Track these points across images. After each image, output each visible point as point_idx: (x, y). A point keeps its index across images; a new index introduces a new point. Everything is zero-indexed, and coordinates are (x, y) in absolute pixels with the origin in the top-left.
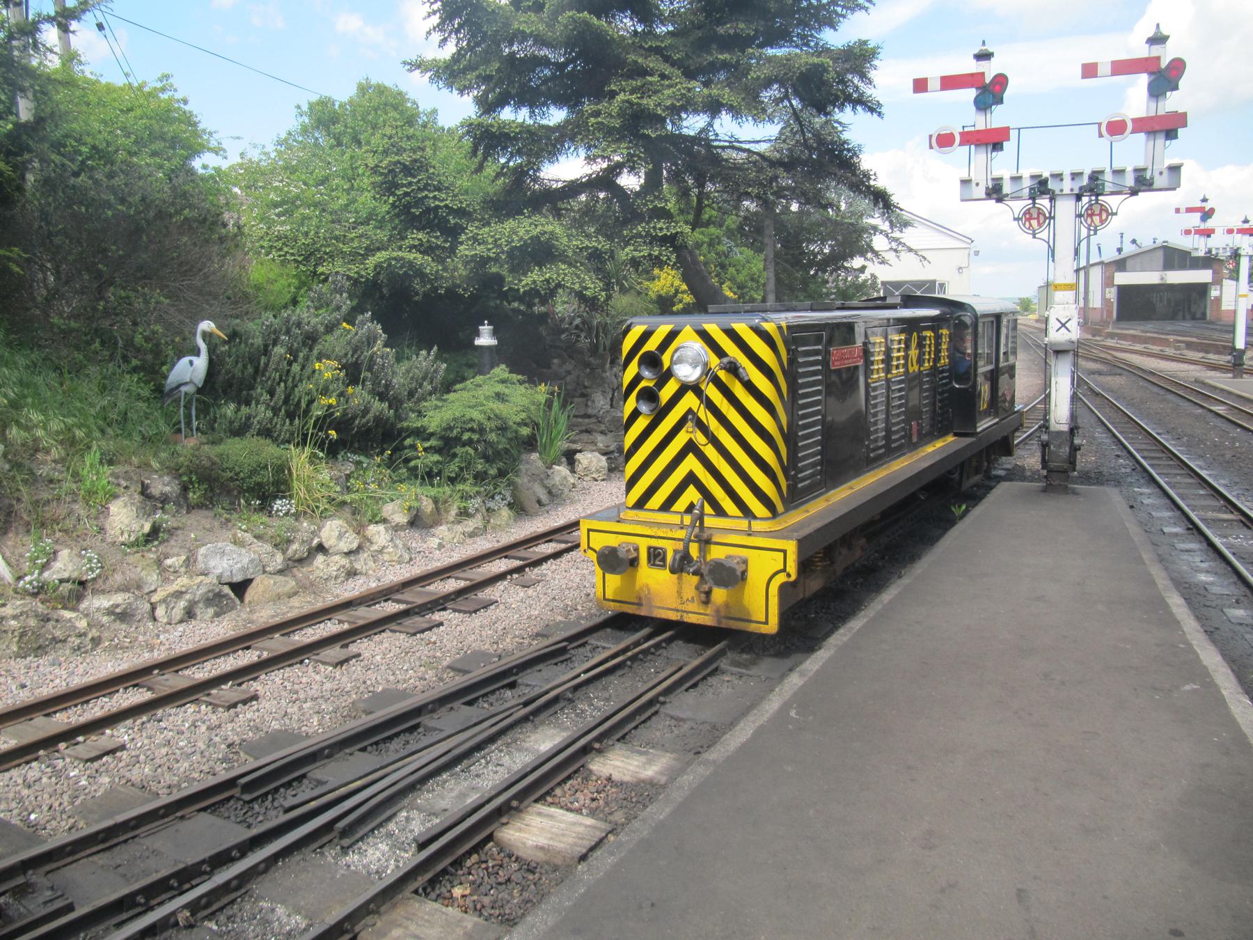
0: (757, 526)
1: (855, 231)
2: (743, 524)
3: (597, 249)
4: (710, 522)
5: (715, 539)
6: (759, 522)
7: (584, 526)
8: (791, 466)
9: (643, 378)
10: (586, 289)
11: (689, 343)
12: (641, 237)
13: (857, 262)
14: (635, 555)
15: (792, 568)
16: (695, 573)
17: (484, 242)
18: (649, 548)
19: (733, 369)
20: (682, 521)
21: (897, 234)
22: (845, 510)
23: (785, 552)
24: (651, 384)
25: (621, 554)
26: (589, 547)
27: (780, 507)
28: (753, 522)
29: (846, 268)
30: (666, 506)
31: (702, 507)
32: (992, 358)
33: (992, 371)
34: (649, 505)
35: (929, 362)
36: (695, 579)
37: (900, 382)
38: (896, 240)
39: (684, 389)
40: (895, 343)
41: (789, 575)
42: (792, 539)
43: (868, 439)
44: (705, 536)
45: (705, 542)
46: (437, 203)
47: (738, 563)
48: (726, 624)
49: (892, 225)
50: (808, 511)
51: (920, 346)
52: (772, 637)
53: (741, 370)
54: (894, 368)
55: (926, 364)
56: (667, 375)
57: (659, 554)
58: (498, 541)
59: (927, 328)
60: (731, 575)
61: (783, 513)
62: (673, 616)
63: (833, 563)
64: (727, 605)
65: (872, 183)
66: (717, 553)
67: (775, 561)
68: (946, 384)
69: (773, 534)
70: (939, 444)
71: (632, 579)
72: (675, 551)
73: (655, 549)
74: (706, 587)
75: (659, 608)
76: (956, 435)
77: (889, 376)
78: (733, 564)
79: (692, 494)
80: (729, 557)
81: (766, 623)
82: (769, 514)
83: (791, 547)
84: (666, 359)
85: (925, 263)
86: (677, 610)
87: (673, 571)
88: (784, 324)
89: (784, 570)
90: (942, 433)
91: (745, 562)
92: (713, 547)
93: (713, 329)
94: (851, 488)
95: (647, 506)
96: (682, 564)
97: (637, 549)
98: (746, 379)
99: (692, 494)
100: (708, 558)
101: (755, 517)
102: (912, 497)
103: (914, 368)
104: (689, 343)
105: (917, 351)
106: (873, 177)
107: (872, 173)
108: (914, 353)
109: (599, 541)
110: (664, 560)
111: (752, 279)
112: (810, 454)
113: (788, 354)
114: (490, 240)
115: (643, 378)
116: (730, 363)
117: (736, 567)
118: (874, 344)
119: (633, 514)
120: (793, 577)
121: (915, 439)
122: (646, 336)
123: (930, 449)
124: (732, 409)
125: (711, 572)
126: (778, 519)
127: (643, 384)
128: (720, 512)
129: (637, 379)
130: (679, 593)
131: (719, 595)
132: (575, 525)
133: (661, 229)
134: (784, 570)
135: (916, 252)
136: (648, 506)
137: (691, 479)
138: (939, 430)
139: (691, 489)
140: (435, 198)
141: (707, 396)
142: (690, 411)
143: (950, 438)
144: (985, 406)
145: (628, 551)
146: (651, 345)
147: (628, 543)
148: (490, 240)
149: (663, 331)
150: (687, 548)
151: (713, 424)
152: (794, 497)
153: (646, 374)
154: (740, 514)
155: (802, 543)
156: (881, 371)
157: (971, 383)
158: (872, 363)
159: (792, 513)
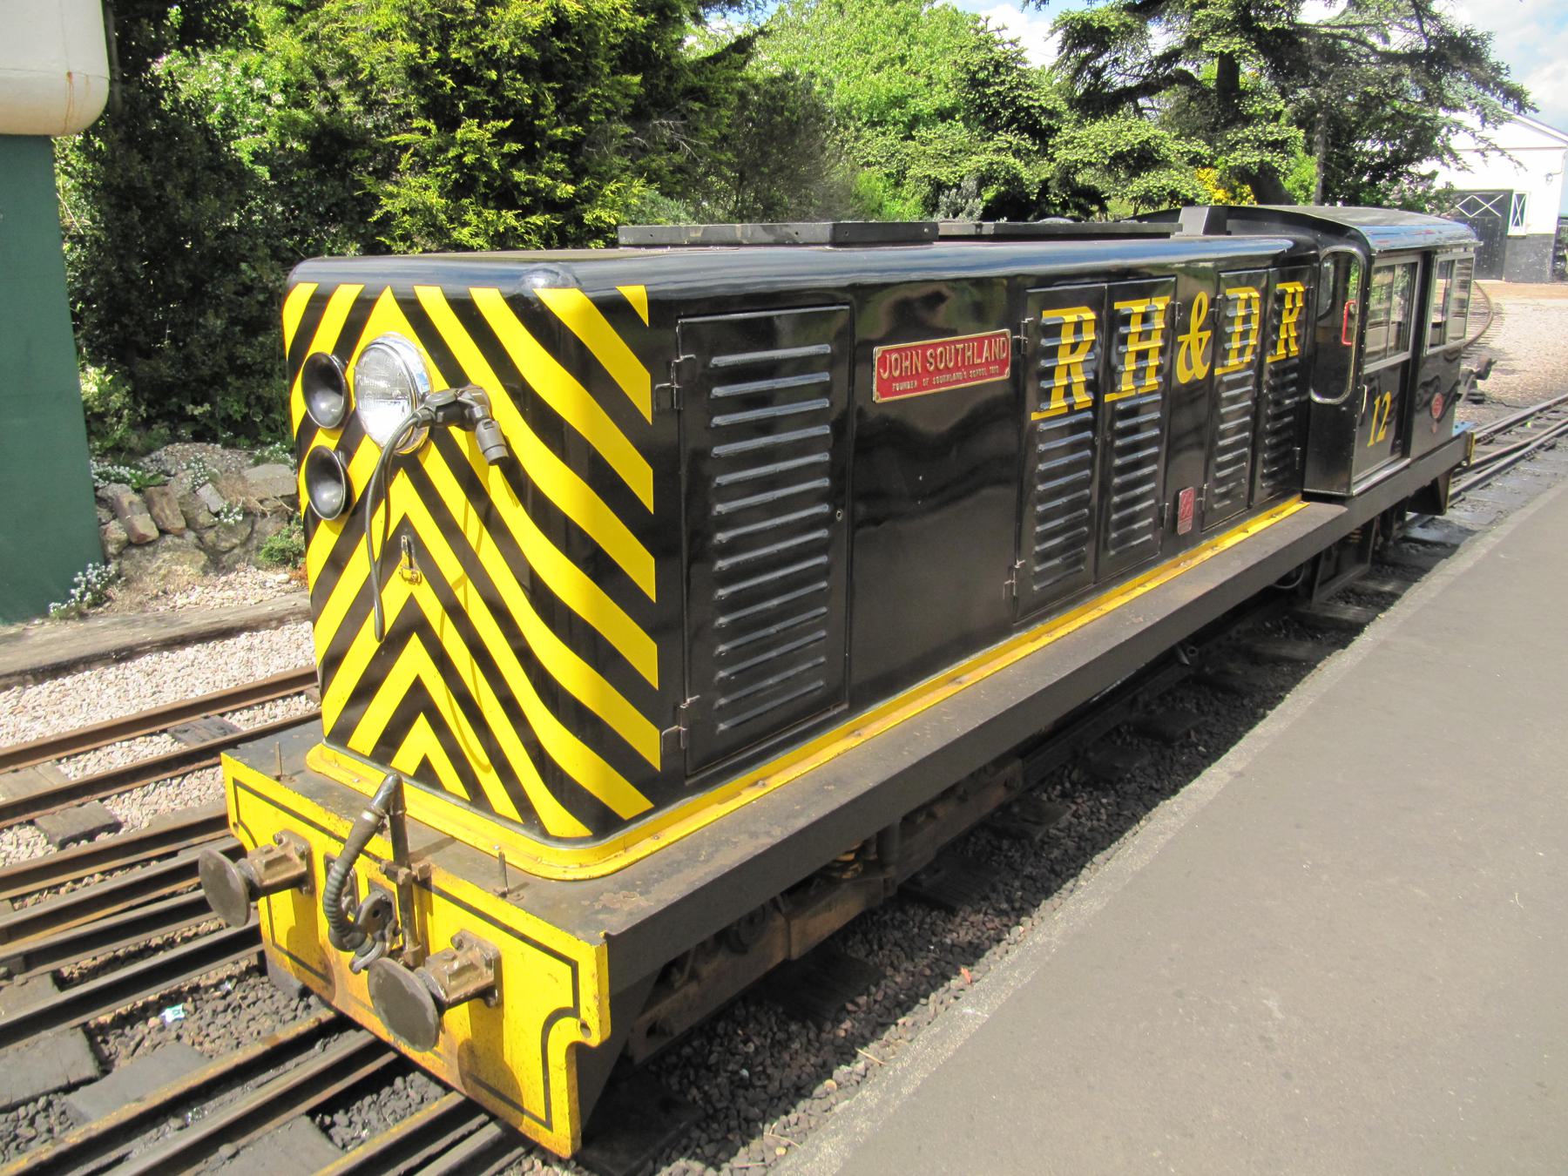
1: (1429, 128)
3: (1198, 154)
10: (1198, 196)
12: (1248, 141)
13: (1425, 167)
17: (1085, 146)
21: (1488, 132)
29: (1410, 174)
33: (1405, 364)
38: (1483, 140)
46: (1031, 103)
49: (1484, 119)
54: (1233, 354)
55: (1233, 361)
65: (1505, 79)
76: (1307, 497)
83: (589, 956)
85: (1521, 170)
88: (636, 294)
90: (1282, 492)
93: (434, 302)
102: (1167, 659)
103: (1191, 368)
105: (1207, 335)
106: (1504, 72)
107: (1503, 66)
111: (1302, 187)
114: (1091, 144)
121: (1184, 527)
133: (1271, 133)
134: (574, 1011)
135: (1503, 152)
140: (1028, 98)
143: (1294, 506)
148: (1091, 144)
157: (1345, 396)
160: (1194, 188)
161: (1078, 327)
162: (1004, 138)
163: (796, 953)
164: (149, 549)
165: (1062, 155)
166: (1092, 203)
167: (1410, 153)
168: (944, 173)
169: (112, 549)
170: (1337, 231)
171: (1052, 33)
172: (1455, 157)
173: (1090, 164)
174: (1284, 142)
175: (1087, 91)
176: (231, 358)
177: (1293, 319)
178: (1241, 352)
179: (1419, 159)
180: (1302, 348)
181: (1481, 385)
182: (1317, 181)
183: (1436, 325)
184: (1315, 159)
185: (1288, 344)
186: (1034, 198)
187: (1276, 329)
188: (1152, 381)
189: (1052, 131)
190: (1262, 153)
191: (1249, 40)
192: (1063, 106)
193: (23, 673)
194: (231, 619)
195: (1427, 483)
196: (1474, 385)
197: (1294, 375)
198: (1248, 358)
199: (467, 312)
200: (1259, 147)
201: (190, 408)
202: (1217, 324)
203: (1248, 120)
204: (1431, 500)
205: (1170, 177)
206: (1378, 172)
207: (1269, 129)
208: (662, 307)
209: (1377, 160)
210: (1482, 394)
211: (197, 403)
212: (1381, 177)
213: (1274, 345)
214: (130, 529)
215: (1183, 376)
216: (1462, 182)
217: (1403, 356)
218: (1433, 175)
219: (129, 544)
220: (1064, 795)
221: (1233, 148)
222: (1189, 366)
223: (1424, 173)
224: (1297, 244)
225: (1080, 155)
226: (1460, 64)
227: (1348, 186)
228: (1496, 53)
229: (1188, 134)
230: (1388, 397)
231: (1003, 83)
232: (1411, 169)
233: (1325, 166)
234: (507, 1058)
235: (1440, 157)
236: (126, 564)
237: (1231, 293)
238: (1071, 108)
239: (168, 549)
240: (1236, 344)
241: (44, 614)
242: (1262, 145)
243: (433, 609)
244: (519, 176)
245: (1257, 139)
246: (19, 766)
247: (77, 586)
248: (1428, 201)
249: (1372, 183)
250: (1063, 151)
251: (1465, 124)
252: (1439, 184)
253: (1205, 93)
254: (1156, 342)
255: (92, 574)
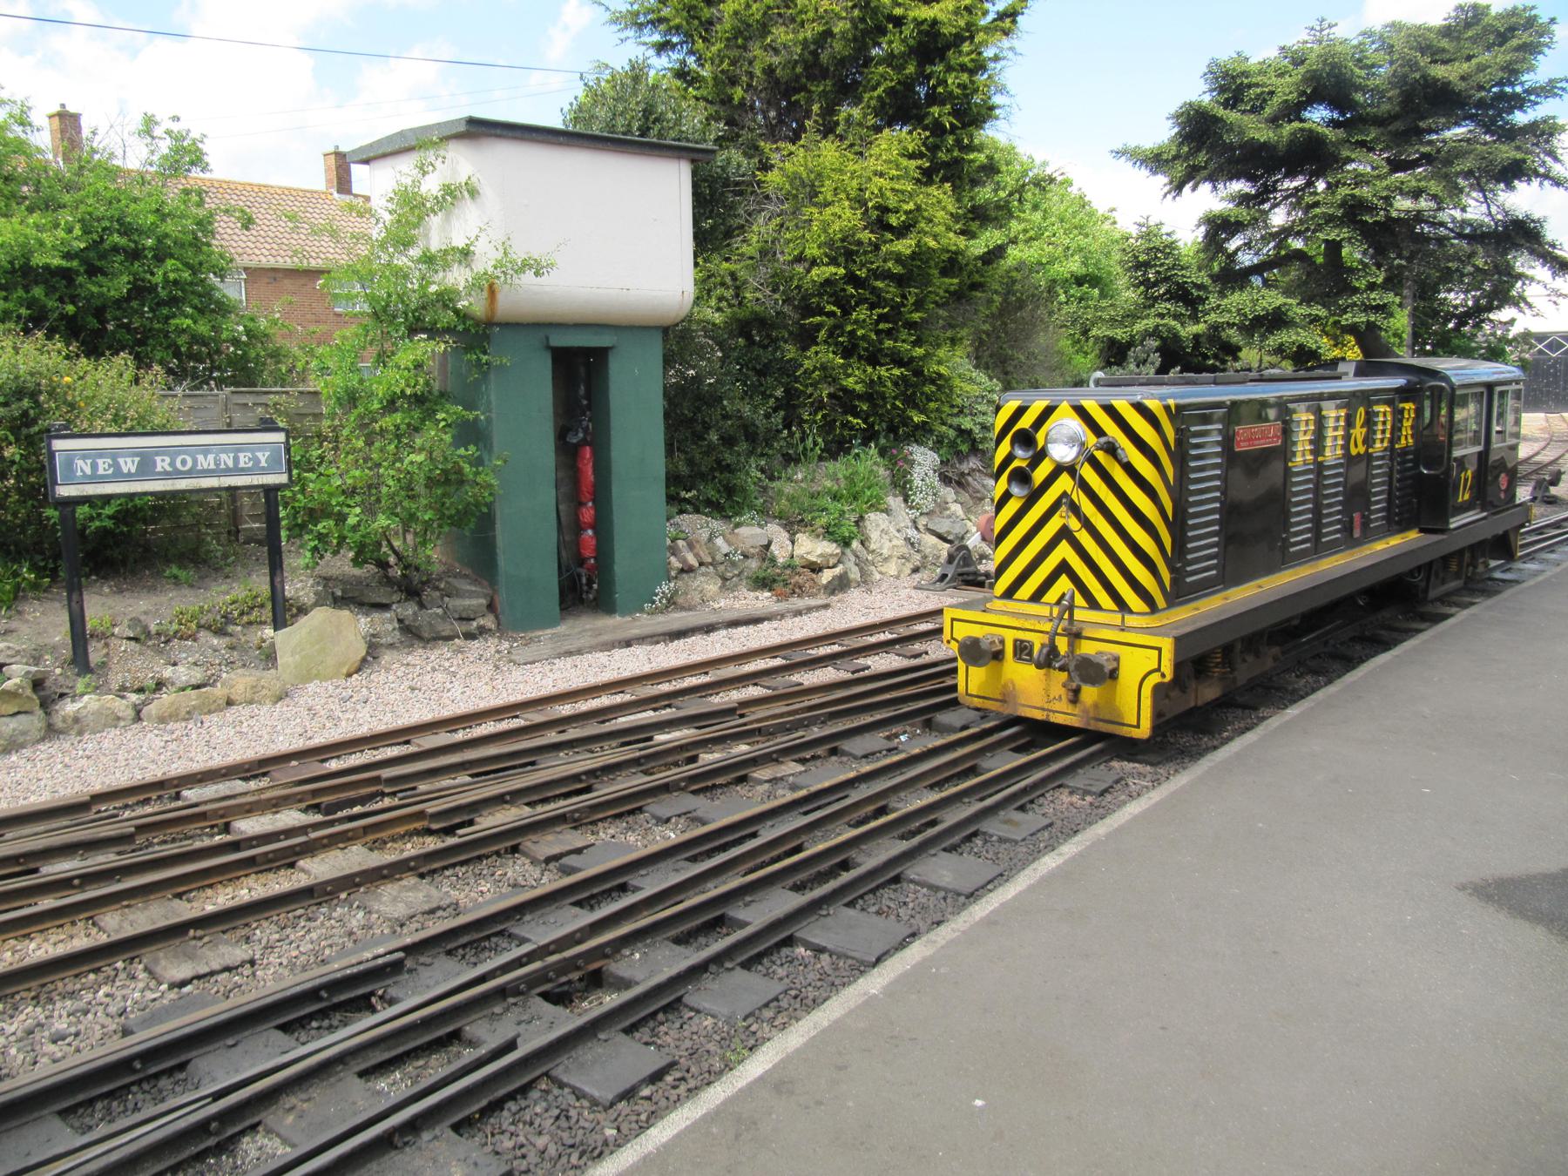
0: (1131, 620)
2: (1116, 619)
4: (1079, 615)
5: (1085, 634)
6: (1135, 617)
7: (948, 616)
8: (1178, 556)
9: (1015, 458)
11: (1066, 423)
13: (1505, 314)
14: (1000, 647)
15: (1168, 668)
16: (1062, 669)
17: (1229, 311)
18: (1016, 641)
19: (1111, 449)
20: (1051, 613)
22: (1243, 609)
23: (1159, 650)
24: (1024, 464)
25: (984, 646)
26: (953, 638)
27: (1160, 602)
28: (1127, 617)
30: (1037, 597)
31: (1072, 597)
32: (1480, 438)
33: (1480, 453)
34: (1018, 595)
35: (1382, 441)
36: (1064, 676)
37: (1382, 458)
39: (1059, 469)
40: (1303, 424)
41: (1163, 675)
42: (1168, 636)
43: (1286, 530)
44: (1074, 629)
45: (1075, 636)
47: (1108, 660)
48: (1093, 726)
50: (1197, 609)
51: (1369, 422)
52: (1148, 740)
53: (1119, 451)
54: (1378, 442)
55: (1378, 445)
56: (1040, 456)
57: (1026, 647)
58: (757, 598)
59: (1378, 402)
60: (1101, 673)
61: (1164, 609)
62: (1038, 715)
63: (1233, 670)
64: (1096, 706)
66: (1087, 648)
67: (1148, 660)
68: (1410, 469)
69: (1163, 630)
70: (1395, 541)
71: (997, 675)
72: (1043, 645)
73: (1022, 641)
74: (1074, 685)
75: (1024, 705)
76: (1421, 531)
77: (1371, 450)
78: (1102, 660)
79: (1064, 584)
80: (1100, 653)
81: (1138, 726)
82: (1147, 609)
83: (1167, 645)
84: (1040, 437)
86: (1043, 709)
87: (1039, 666)
89: (1158, 670)
90: (1403, 527)
91: (1117, 659)
92: (1083, 642)
93: (1091, 406)
94: (1260, 587)
95: (1016, 596)
96: (1049, 659)
97: (1002, 642)
98: (1125, 460)
99: (1064, 584)
100: (1078, 652)
101: (1131, 612)
102: (1349, 600)
104: (1066, 423)
105: (1364, 430)
108: (1358, 432)
109: (962, 631)
110: (1030, 654)
112: (1205, 541)
113: (1176, 434)
115: (1015, 458)
116: (1109, 443)
117: (1105, 663)
118: (1299, 422)
119: (999, 604)
120: (1168, 678)
121: (1357, 534)
122: (1020, 412)
123: (1379, 546)
124: (1110, 493)
125: (1077, 667)
126: (1156, 616)
127: (1016, 464)
128: (1093, 604)
129: (1009, 458)
130: (1047, 690)
131: (1090, 693)
132: (939, 612)
134: (1158, 670)
136: (1017, 596)
137: (1064, 568)
138: (1396, 523)
139: (1064, 579)
140: (1183, 276)
141: (1080, 476)
142: (1065, 494)
143: (1413, 535)
144: (1467, 497)
145: (993, 643)
146: (1025, 422)
147: (993, 635)
149: (1038, 407)
150: (1052, 641)
151: (1088, 508)
152: (1179, 593)
153: (1019, 452)
154: (1116, 608)
155: (1178, 640)
156: (1307, 453)
157: (1443, 469)
158: (1311, 442)
159: (1174, 611)
160: (1316, 342)
161: (1307, 422)
162: (1163, 307)
163: (1200, 703)
164: (692, 575)
165: (1213, 317)
166: (1227, 354)
167: (1490, 303)
168: (1120, 334)
169: (673, 573)
170: (1434, 374)
171: (1198, 226)
172: (1530, 306)
173: (1234, 324)
174: (1385, 305)
175: (1222, 269)
176: (719, 462)
177: (1410, 423)
178: (1382, 441)
179: (1499, 308)
180: (1416, 442)
181: (1553, 490)
182: (1409, 330)
183: (1498, 432)
184: (1406, 312)
185: (1406, 440)
186: (1189, 350)
187: (1400, 430)
188: (1339, 452)
189: (1202, 300)
190: (1367, 315)
191: (1355, 230)
192: (1207, 281)
193: (664, 634)
194: (759, 613)
195: (1501, 532)
196: (1547, 489)
197: (1411, 457)
198: (1385, 444)
199: (1110, 410)
200: (1365, 311)
201: (683, 494)
202: (1369, 422)
203: (1355, 290)
204: (1503, 547)
205: (1298, 334)
206: (1462, 319)
207: (1372, 296)
208: (1179, 408)
209: (1461, 309)
210: (1554, 497)
211: (688, 491)
212: (1465, 324)
213: (1399, 438)
214: (684, 561)
215: (1354, 451)
216: (1537, 326)
217: (1479, 448)
218: (1512, 322)
219: (682, 571)
220: (1297, 676)
221: (1344, 311)
222: (1356, 446)
223: (1504, 319)
224: (1409, 381)
225: (1226, 318)
226: (1523, 242)
227: (1435, 333)
228: (1550, 234)
229: (1307, 300)
230: (1469, 473)
231: (1162, 265)
232: (1491, 316)
233: (1414, 315)
234: (1118, 700)
235: (1516, 305)
236: (680, 583)
237: (1376, 408)
238: (1214, 282)
239: (703, 575)
240: (1379, 436)
241: (642, 610)
242: (1367, 308)
243: (1074, 524)
244: (889, 343)
245: (1363, 303)
246: (133, 902)
247: (656, 595)
248: (1509, 342)
249: (1457, 329)
250: (1213, 315)
251: (1538, 278)
252: (1514, 331)
253: (1317, 268)
254: (1340, 432)
255: (665, 588)
